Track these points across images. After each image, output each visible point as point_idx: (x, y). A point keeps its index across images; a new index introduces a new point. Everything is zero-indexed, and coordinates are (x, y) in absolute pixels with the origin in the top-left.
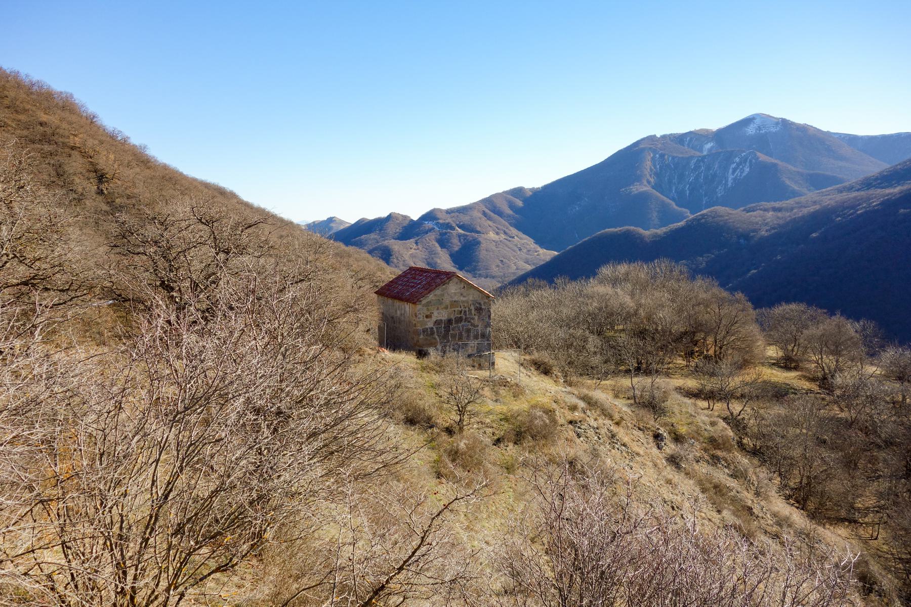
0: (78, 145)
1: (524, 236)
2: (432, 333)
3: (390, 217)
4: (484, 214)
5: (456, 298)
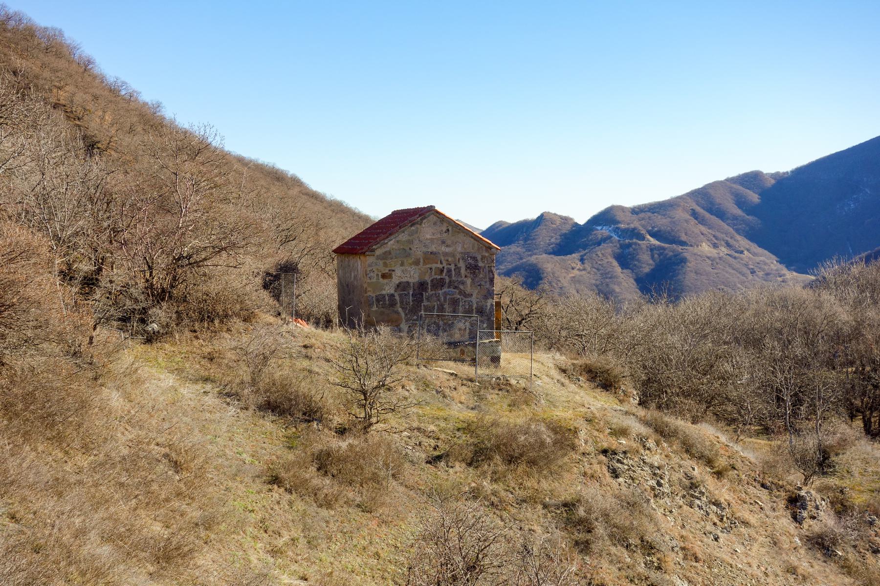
0: (62, 102)
1: (760, 250)
2: (393, 304)
3: (541, 218)
4: (694, 214)
5: (433, 248)
